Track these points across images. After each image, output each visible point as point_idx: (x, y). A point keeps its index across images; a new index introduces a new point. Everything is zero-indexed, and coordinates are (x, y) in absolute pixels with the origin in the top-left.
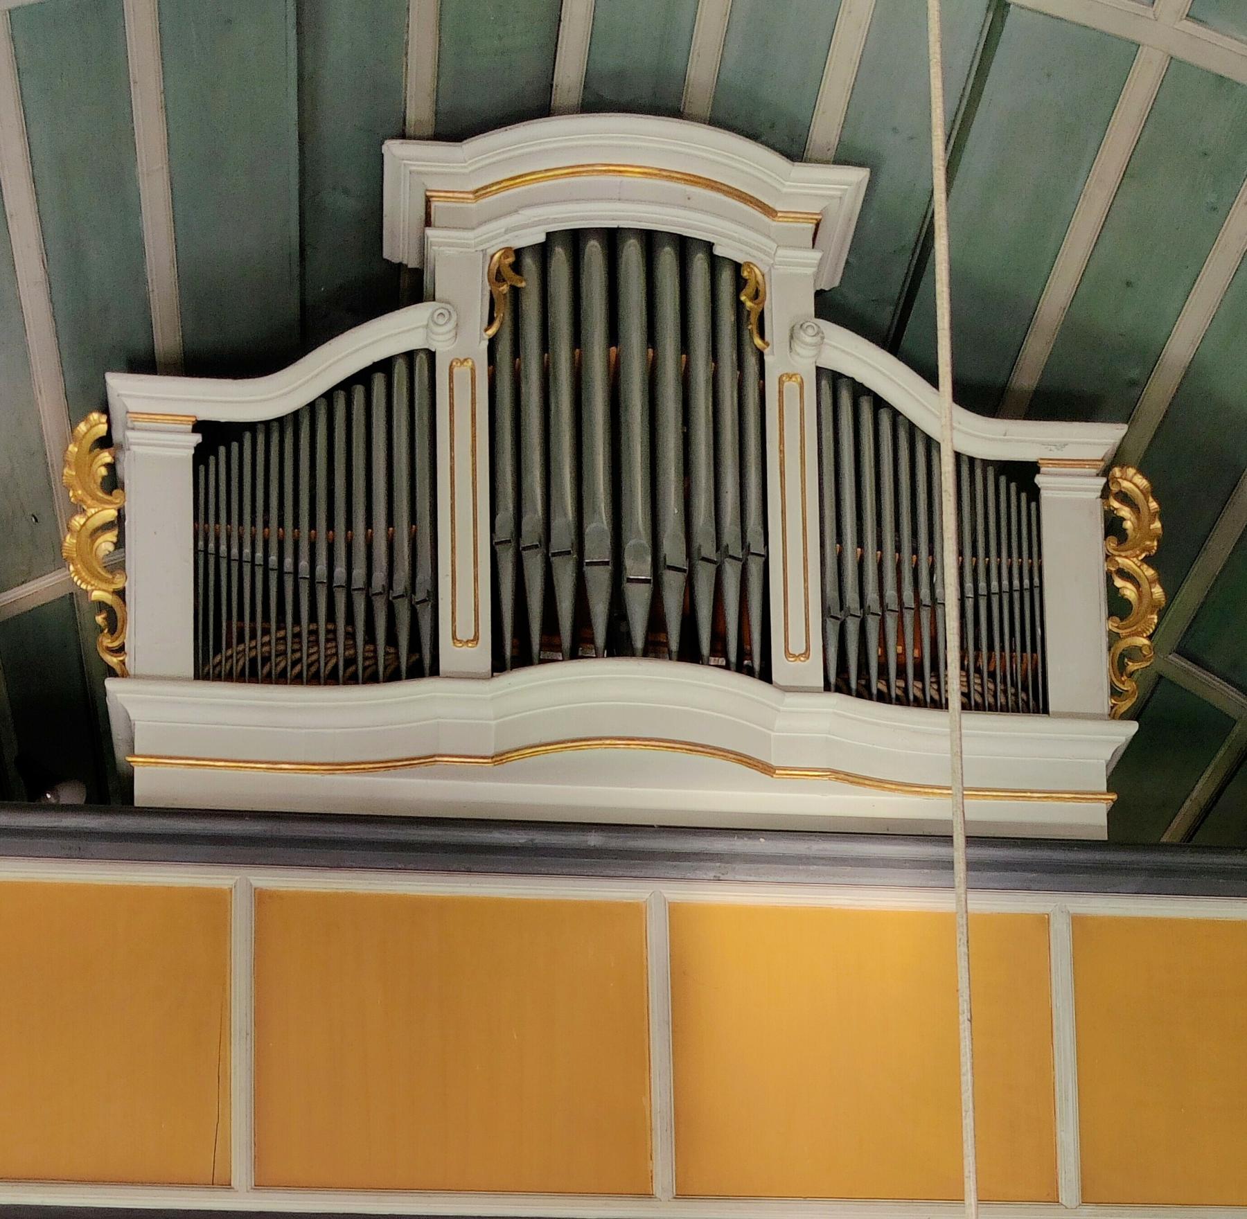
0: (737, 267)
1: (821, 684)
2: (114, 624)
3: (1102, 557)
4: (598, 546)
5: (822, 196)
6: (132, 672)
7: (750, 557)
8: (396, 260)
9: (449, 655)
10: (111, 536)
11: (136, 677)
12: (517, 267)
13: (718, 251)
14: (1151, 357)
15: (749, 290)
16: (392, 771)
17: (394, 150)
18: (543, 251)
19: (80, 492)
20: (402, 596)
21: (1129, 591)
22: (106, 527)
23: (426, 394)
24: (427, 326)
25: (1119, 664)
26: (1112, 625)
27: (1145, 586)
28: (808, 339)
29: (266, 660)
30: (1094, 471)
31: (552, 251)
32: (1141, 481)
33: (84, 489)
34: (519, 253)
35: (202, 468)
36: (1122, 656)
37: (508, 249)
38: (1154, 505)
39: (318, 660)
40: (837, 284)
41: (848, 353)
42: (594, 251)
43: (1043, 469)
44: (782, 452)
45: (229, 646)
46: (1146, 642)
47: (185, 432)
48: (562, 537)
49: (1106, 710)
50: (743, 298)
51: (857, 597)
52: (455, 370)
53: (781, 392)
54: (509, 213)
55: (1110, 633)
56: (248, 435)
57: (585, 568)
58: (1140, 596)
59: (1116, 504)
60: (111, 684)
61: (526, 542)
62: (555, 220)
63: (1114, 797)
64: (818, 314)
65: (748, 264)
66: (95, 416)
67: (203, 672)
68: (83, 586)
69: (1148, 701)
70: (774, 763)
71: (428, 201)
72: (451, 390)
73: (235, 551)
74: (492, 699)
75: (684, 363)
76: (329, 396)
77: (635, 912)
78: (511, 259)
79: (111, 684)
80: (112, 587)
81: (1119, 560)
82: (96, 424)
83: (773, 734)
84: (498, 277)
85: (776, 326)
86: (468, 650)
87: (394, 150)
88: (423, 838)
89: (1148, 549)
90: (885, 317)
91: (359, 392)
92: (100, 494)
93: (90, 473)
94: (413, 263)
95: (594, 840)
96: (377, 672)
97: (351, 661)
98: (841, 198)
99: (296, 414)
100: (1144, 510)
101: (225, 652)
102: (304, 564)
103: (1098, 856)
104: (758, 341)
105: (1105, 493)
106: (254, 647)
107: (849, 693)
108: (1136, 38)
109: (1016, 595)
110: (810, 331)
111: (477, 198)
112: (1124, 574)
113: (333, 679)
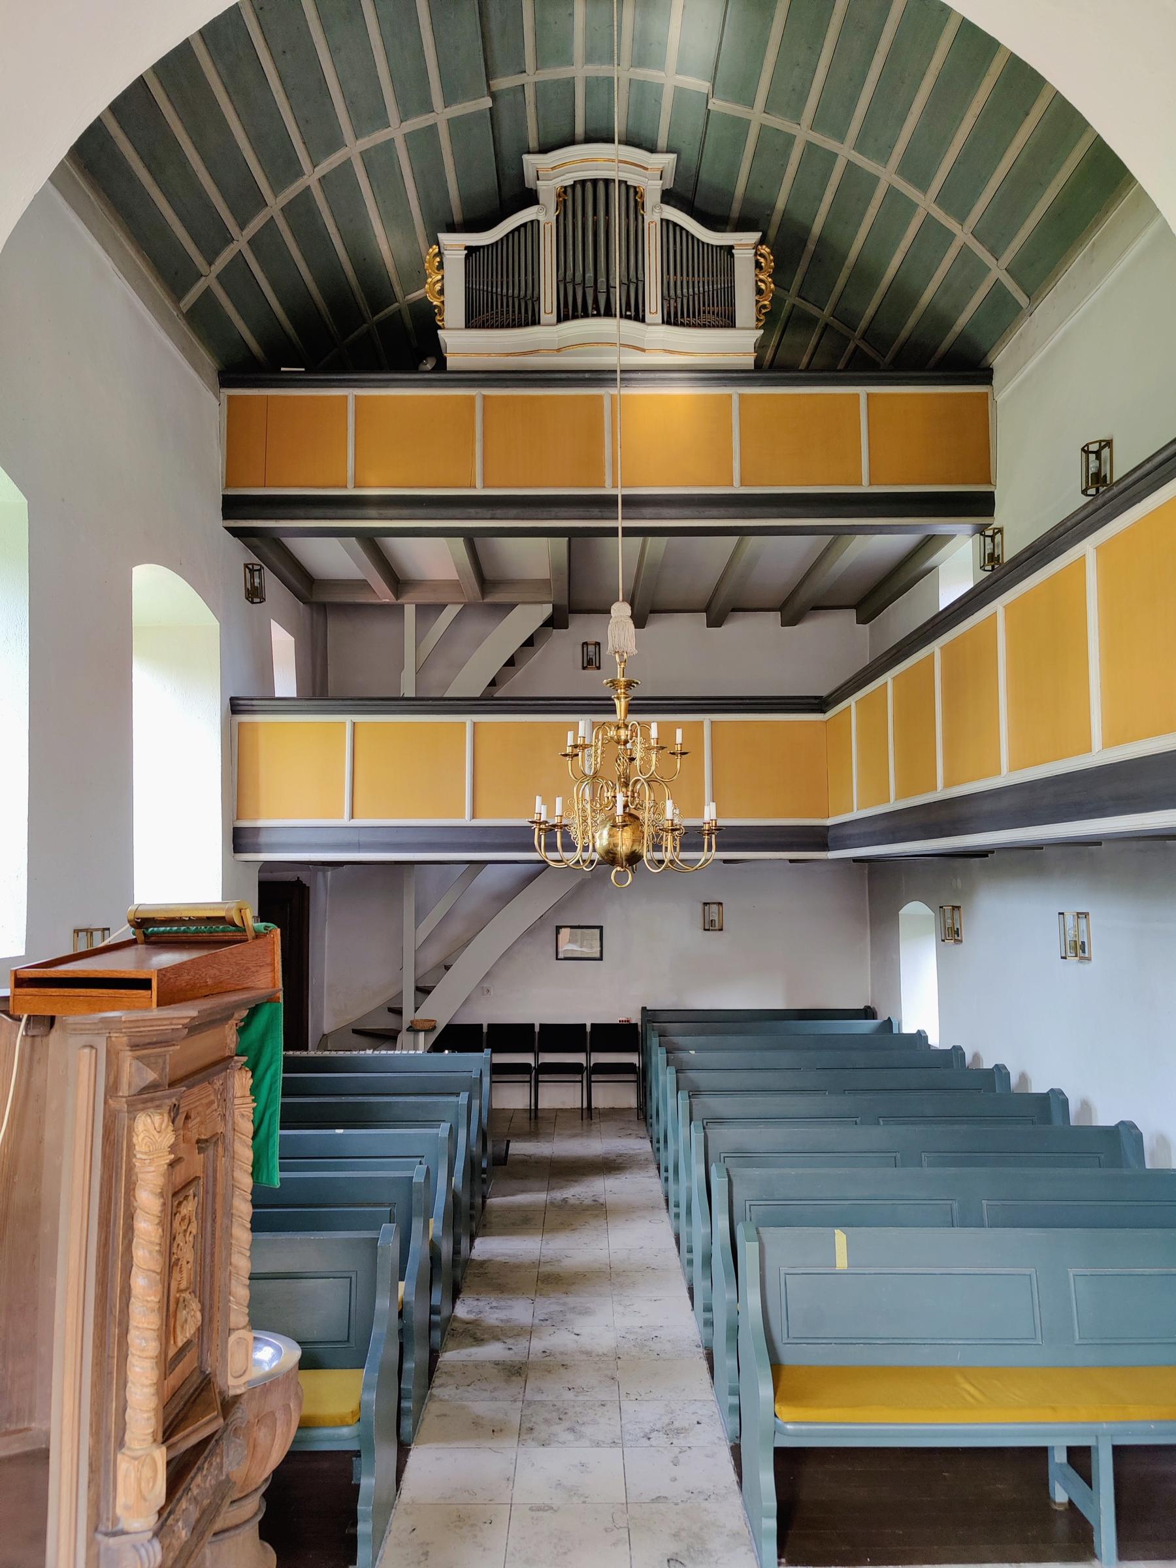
0: (635, 188)
1: (661, 322)
2: (441, 313)
3: (754, 275)
8: (529, 187)
9: (544, 318)
10: (440, 284)
12: (565, 192)
13: (629, 183)
14: (772, 207)
15: (639, 195)
17: (526, 157)
18: (573, 186)
21: (763, 286)
22: (438, 281)
23: (537, 235)
24: (536, 213)
25: (759, 311)
26: (757, 298)
27: (768, 284)
28: (657, 211)
29: (487, 320)
30: (752, 247)
32: (768, 250)
36: (760, 308)
37: (562, 187)
38: (772, 258)
40: (672, 186)
42: (589, 185)
44: (649, 247)
45: (476, 317)
47: (462, 250)
48: (579, 279)
49: (754, 326)
51: (667, 293)
52: (546, 226)
53: (649, 227)
54: (562, 175)
55: (757, 301)
56: (482, 250)
59: (759, 258)
60: (439, 332)
61: (568, 280)
62: (576, 177)
63: (756, 354)
64: (661, 202)
65: (639, 187)
66: (434, 247)
67: (469, 325)
70: (646, 348)
71: (537, 171)
73: (478, 287)
76: (507, 236)
77: (600, 397)
79: (439, 332)
80: (440, 301)
82: (435, 249)
84: (559, 196)
85: (648, 206)
89: (770, 272)
91: (516, 234)
92: (436, 271)
93: (433, 265)
94: (535, 189)
95: (587, 375)
96: (521, 323)
97: (514, 320)
100: (769, 260)
101: (475, 319)
102: (499, 290)
104: (642, 212)
105: (756, 254)
108: (750, 119)
110: (658, 208)
112: (762, 281)
113: (508, 326)
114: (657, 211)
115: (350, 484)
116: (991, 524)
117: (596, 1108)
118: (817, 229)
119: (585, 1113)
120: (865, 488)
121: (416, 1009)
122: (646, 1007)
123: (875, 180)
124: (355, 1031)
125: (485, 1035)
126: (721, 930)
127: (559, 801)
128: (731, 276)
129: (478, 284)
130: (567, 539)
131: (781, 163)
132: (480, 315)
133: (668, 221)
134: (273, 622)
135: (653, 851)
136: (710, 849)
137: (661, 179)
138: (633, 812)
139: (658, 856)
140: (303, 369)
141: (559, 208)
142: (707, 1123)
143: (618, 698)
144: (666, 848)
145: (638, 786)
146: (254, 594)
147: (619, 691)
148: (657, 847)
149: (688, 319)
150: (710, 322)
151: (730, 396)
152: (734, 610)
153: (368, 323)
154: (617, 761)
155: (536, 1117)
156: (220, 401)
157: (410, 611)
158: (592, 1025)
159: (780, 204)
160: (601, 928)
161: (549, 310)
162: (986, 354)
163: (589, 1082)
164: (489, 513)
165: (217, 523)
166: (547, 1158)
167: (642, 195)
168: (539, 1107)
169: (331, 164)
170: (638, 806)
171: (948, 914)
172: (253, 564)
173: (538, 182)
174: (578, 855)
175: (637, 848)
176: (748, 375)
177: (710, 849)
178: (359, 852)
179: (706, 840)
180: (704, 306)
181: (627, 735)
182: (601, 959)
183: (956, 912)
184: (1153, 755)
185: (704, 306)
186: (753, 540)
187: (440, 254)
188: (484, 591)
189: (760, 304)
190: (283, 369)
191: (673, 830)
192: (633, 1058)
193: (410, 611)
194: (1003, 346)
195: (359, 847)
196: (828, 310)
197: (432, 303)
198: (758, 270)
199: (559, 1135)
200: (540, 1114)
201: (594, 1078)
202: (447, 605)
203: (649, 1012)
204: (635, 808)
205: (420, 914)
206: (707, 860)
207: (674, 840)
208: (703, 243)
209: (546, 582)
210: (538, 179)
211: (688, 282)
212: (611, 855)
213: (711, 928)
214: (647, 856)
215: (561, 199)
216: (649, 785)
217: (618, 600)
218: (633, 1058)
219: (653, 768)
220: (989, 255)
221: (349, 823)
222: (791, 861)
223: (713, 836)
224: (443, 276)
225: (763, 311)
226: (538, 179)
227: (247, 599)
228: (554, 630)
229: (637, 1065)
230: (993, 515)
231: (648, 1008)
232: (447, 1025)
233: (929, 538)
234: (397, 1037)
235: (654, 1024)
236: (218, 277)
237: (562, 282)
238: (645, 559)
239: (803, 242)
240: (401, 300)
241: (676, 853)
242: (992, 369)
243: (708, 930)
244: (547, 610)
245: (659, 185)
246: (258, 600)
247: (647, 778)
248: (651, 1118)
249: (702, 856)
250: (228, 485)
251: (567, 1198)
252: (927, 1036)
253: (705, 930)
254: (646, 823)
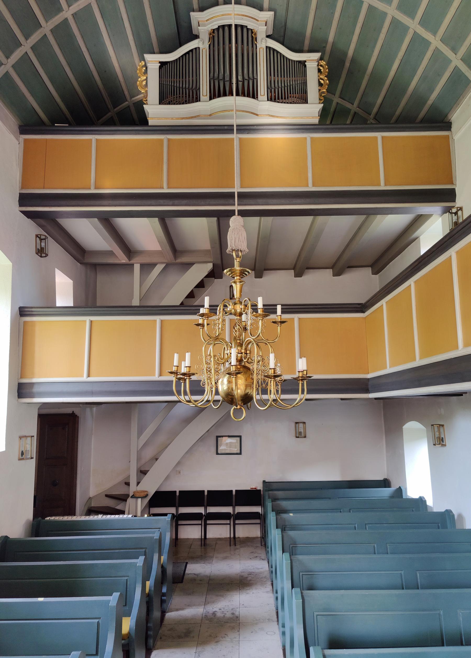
0: (252, 30)
1: (267, 100)
3: (317, 76)
4: (227, 78)
5: (266, 17)
6: (148, 104)
7: (272, 89)
10: (145, 82)
11: (149, 105)
12: (213, 32)
14: (326, 42)
15: (254, 33)
16: (192, 118)
17: (192, 14)
18: (218, 29)
19: (140, 74)
20: (194, 89)
21: (322, 82)
25: (320, 95)
26: (319, 88)
27: (325, 81)
28: (264, 41)
31: (220, 29)
32: (324, 63)
33: (140, 74)
34: (214, 30)
35: (161, 70)
38: (327, 67)
39: (180, 101)
41: (271, 43)
42: (226, 28)
43: (307, 62)
44: (260, 61)
45: (165, 99)
46: (325, 90)
48: (221, 77)
49: (318, 103)
50: (253, 35)
52: (203, 50)
53: (260, 51)
57: (225, 82)
58: (324, 82)
59: (320, 67)
62: (219, 24)
65: (253, 29)
66: (142, 62)
67: (161, 103)
68: (140, 90)
69: (336, 108)
72: (202, 54)
73: (166, 83)
74: (209, 105)
75: (242, 47)
76: (182, 56)
78: (212, 31)
79: (144, 106)
81: (320, 76)
82: (143, 63)
83: (258, 109)
84: (210, 34)
86: (205, 97)
87: (192, 14)
88: (197, 129)
90: (281, 39)
91: (187, 55)
98: (270, 17)
99: (177, 59)
100: (325, 68)
103: (317, 127)
104: (255, 42)
105: (318, 65)
106: (170, 99)
107: (272, 101)
109: (302, 84)
110: (264, 40)
111: (207, 22)
114: (264, 41)
115: (92, 187)
116: (455, 206)
117: (238, 537)
118: (351, 53)
119: (232, 540)
120: (382, 187)
121: (138, 483)
122: (265, 481)
123: (386, 14)
124: (107, 496)
125: (177, 497)
126: (305, 437)
127: (188, 355)
128: (305, 77)
129: (166, 82)
130: (216, 218)
131: (332, 11)
132: (167, 98)
133: (270, 48)
134: (56, 269)
135: (262, 394)
136: (303, 393)
137: (266, 26)
138: (247, 365)
139: (265, 397)
140: (68, 125)
141: (210, 40)
142: (302, 575)
143: (235, 282)
144: (270, 391)
145: (250, 346)
146: (41, 252)
147: (236, 278)
148: (265, 391)
149: (282, 100)
150: (294, 102)
151: (306, 138)
152: (308, 268)
153: (111, 112)
154: (234, 328)
155: (205, 544)
156: (19, 141)
157: (137, 268)
158: (236, 491)
159: (331, 39)
160: (240, 437)
161: (205, 94)
162: (447, 115)
163: (235, 524)
164: (171, 203)
165: (15, 208)
166: (208, 577)
167: (255, 34)
168: (207, 537)
169: (79, 5)
170: (250, 360)
171: (436, 429)
172: (41, 235)
173: (199, 27)
174: (206, 397)
175: (249, 391)
176: (315, 127)
177: (303, 393)
178: (92, 397)
179: (300, 384)
180: (290, 93)
181: (241, 309)
182: (240, 453)
183: (441, 429)
184: (464, 356)
185: (290, 93)
186: (321, 219)
187: (146, 66)
188: (175, 257)
189: (321, 91)
190: (56, 125)
191: (275, 376)
192: (258, 509)
193: (137, 268)
194: (458, 107)
195: (92, 394)
196: (356, 103)
197: (141, 91)
198: (319, 74)
199: (216, 558)
200: (208, 542)
201: (237, 522)
202: (158, 264)
203: (267, 483)
204: (247, 361)
205: (140, 432)
206: (301, 400)
207: (277, 385)
208: (289, 59)
209: (207, 251)
210: (199, 26)
211: (281, 81)
212: (230, 397)
213: (300, 436)
214: (256, 397)
215: (211, 36)
216: (257, 345)
217: (235, 215)
218: (258, 509)
219: (260, 331)
220: (450, 51)
221: (87, 379)
222: (342, 399)
223: (305, 382)
224: (147, 77)
225: (323, 95)
226: (199, 26)
227: (37, 254)
228: (215, 279)
229: (261, 513)
230: (455, 202)
231: (266, 481)
232: (156, 492)
233: (419, 216)
234: (127, 500)
235: (270, 492)
236: (13, 66)
237: (212, 79)
238: (260, 237)
239: (343, 62)
240: (129, 101)
241: (278, 396)
242: (451, 123)
243: (298, 437)
244: (209, 267)
245: (265, 29)
246: (43, 255)
247: (256, 338)
248: (268, 548)
249: (298, 397)
250: (23, 187)
251: (216, 611)
252: (426, 500)
253: (297, 437)
254: (255, 372)
